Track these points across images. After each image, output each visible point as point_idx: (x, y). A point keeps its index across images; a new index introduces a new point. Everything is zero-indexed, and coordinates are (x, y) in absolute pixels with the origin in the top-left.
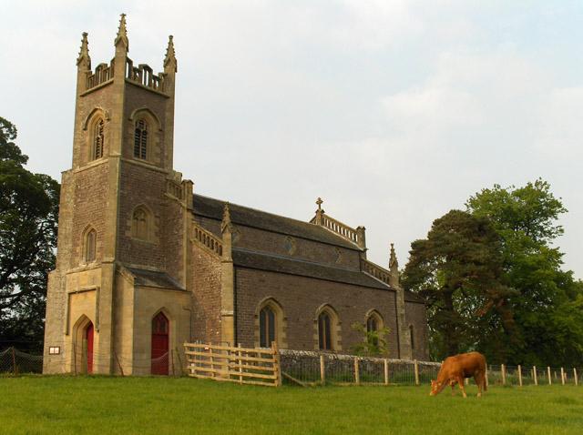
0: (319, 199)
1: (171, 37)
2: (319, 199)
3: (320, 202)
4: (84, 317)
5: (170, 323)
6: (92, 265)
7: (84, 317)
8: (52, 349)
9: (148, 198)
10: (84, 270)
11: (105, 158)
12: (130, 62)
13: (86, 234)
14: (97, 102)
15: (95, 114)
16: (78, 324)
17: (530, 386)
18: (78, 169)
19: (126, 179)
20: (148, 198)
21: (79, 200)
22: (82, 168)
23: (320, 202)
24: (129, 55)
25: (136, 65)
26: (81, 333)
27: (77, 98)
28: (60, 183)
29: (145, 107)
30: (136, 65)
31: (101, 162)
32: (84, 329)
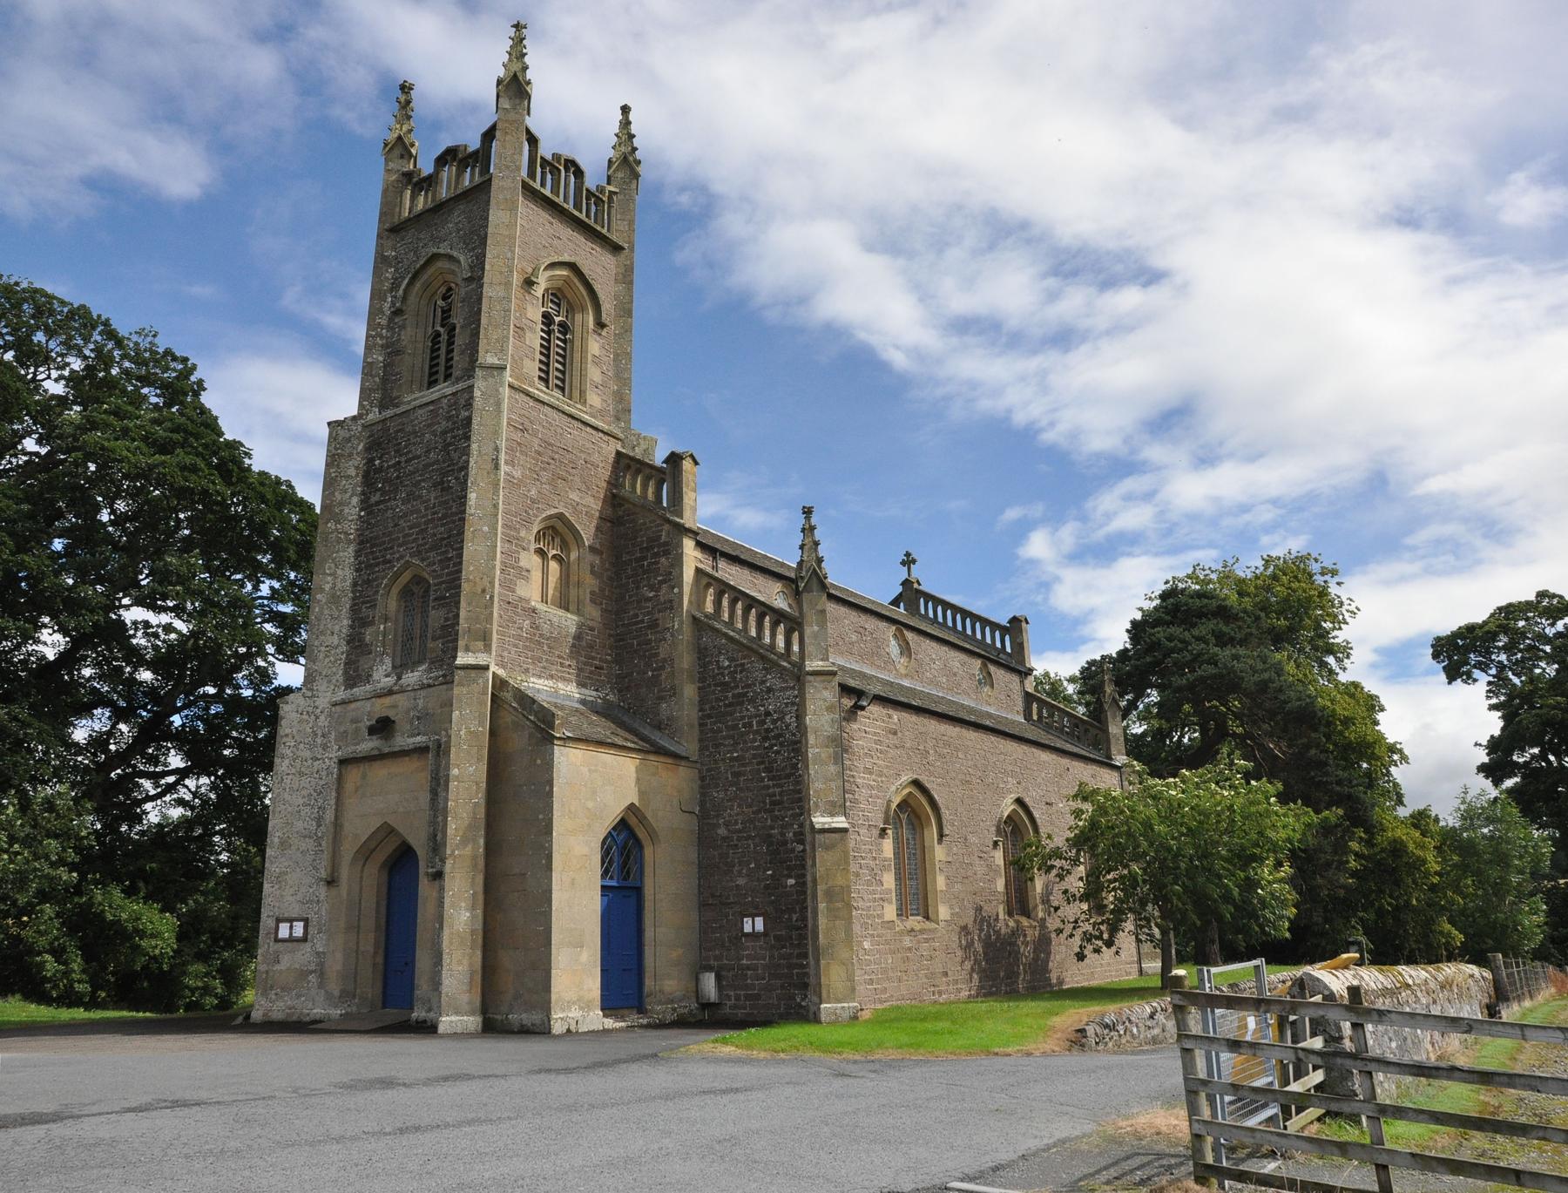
0: (908, 554)
1: (625, 110)
2: (908, 554)
3: (908, 561)
4: (387, 831)
5: (648, 852)
6: (412, 678)
7: (387, 831)
8: (284, 931)
9: (574, 496)
10: (390, 692)
11: (458, 380)
12: (533, 140)
13: (395, 591)
14: (438, 240)
15: (431, 270)
16: (365, 853)
17: (1231, 982)
18: (375, 415)
19: (626, 306)
20: (574, 496)
21: (375, 498)
22: (389, 413)
23: (908, 561)
24: (532, 122)
25: (545, 151)
26: (373, 876)
27: (379, 236)
28: (311, 492)
29: (566, 258)
30: (545, 151)
31: (449, 391)
32: (383, 865)
